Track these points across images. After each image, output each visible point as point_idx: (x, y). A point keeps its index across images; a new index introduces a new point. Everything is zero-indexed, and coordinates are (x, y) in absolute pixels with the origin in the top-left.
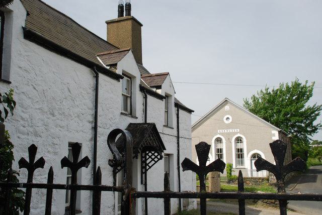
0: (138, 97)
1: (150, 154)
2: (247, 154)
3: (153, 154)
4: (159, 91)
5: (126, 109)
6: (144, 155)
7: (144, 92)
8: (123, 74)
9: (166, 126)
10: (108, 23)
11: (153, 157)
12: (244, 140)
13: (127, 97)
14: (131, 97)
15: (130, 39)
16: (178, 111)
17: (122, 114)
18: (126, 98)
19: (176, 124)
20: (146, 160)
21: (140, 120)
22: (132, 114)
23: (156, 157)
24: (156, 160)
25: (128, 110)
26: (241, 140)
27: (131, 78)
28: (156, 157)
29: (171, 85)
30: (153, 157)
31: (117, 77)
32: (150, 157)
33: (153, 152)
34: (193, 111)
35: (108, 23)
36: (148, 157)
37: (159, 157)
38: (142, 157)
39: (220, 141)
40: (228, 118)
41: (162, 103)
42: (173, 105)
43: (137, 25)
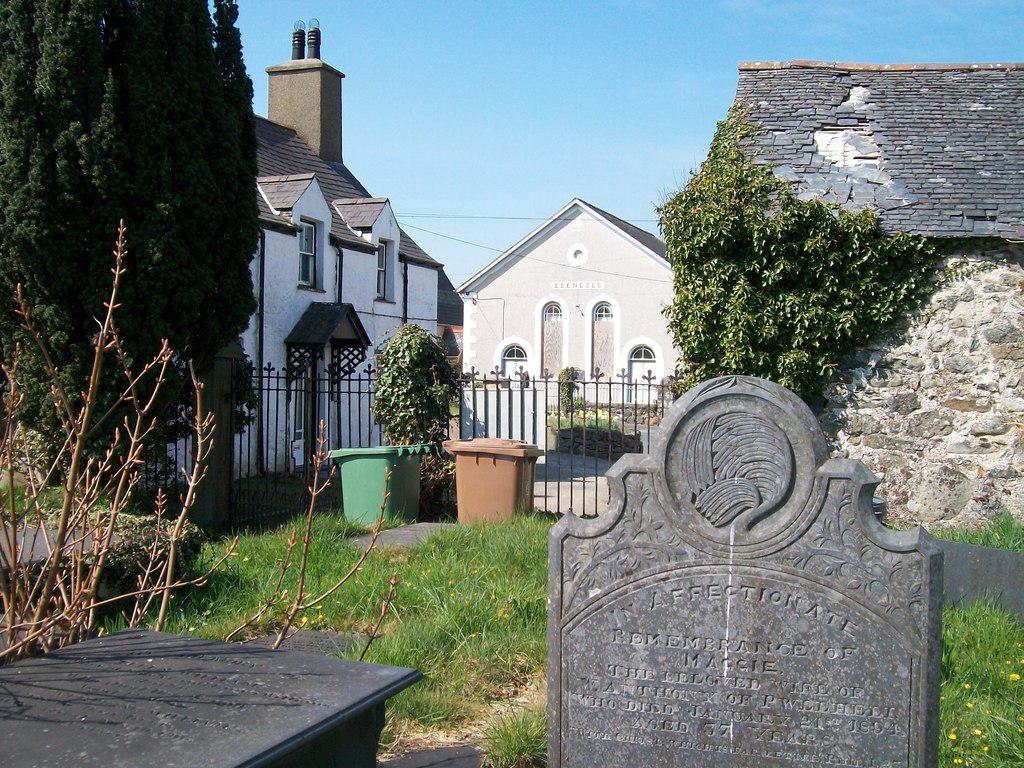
0: (328, 255)
1: (346, 353)
2: (621, 347)
3: (351, 353)
4: (368, 238)
5: (305, 275)
6: (336, 354)
7: (337, 246)
8: (302, 220)
9: (382, 299)
10: (271, 73)
11: (351, 357)
12: (615, 309)
13: (308, 256)
14: (315, 256)
15: (317, 112)
16: (406, 268)
17: (300, 287)
18: (305, 259)
19: (402, 294)
20: (340, 361)
21: (328, 298)
22: (316, 286)
23: (356, 357)
24: (356, 361)
25: (310, 276)
26: (607, 311)
27: (315, 224)
28: (356, 357)
29: (394, 223)
30: (351, 357)
31: (292, 231)
32: (346, 357)
33: (302, 351)
34: (375, 300)
35: (271, 73)
36: (342, 357)
37: (360, 357)
38: (333, 357)
39: (557, 311)
40: (577, 253)
41: (372, 261)
42: (396, 257)
43: (331, 80)
